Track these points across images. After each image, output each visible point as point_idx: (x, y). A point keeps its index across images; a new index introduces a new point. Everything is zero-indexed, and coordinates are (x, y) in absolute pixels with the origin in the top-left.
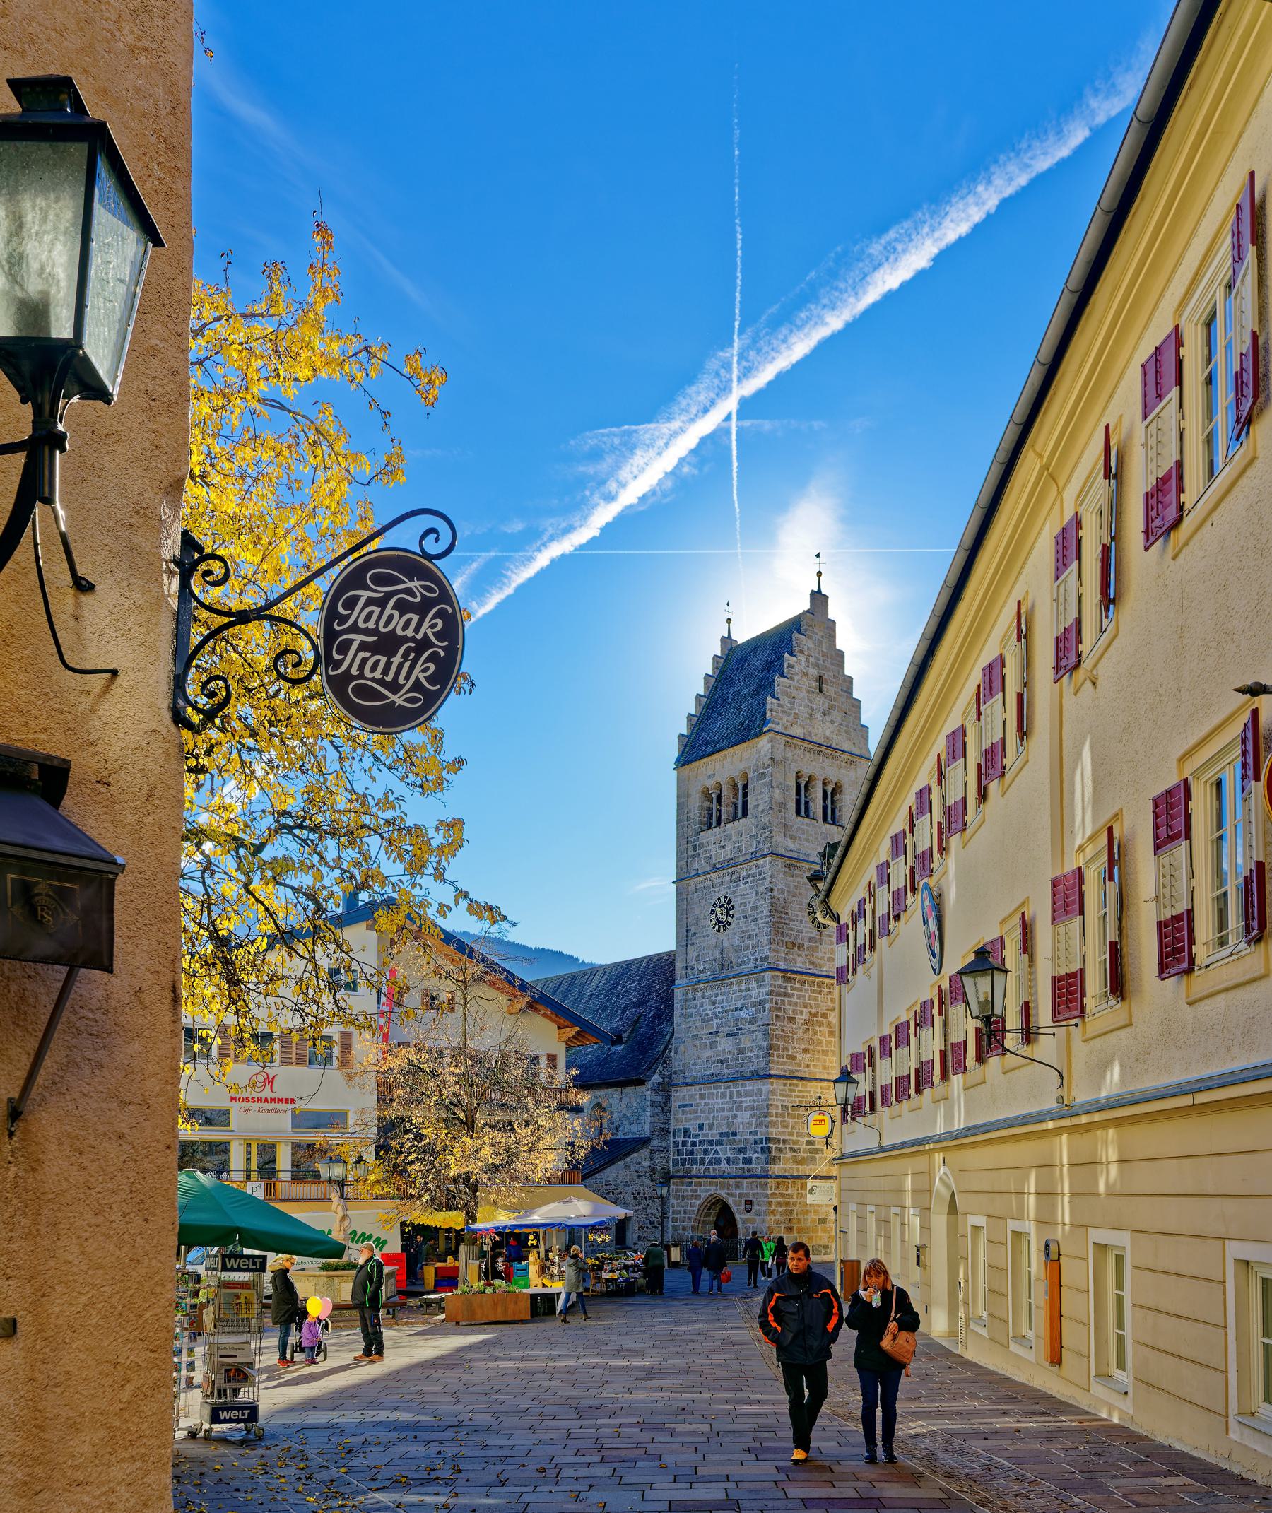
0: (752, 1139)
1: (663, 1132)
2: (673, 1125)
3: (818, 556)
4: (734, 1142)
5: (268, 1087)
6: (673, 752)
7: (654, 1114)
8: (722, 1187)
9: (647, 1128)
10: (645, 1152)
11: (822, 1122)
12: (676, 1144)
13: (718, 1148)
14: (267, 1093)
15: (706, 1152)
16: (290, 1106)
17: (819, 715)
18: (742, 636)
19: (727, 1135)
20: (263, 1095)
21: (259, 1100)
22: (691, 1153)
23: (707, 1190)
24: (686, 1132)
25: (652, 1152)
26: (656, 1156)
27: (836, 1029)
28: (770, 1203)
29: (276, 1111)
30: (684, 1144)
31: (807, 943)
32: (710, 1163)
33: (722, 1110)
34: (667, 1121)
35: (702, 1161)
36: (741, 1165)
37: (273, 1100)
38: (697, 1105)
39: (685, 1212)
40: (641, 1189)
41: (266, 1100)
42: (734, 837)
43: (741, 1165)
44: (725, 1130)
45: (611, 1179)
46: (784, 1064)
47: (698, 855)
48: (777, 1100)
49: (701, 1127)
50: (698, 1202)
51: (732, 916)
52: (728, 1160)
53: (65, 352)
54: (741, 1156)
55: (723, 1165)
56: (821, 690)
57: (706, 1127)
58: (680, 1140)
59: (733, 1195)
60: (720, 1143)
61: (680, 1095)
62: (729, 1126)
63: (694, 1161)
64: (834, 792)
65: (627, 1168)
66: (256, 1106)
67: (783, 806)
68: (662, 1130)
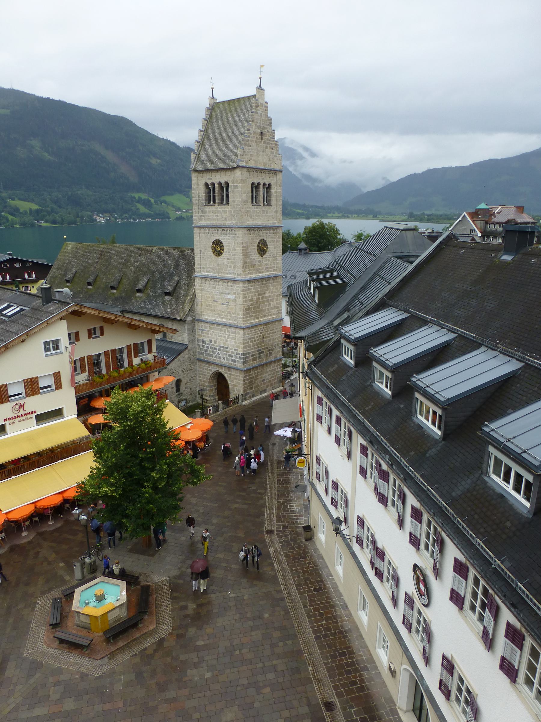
2: (197, 337)
3: (262, 66)
4: (226, 351)
5: (22, 409)
7: (189, 334)
8: (222, 369)
10: (186, 352)
12: (199, 345)
13: (219, 352)
14: (22, 412)
16: (34, 415)
17: (261, 153)
19: (223, 347)
20: (20, 414)
21: (18, 416)
22: (206, 351)
24: (203, 341)
26: (191, 351)
29: (28, 419)
31: (257, 263)
32: (216, 357)
33: (221, 336)
34: (194, 336)
35: (212, 356)
36: (230, 362)
38: (208, 331)
39: (204, 375)
40: (185, 368)
41: (22, 416)
43: (230, 362)
44: (222, 345)
46: (249, 320)
48: (240, 271)
49: (211, 341)
50: (211, 372)
52: (224, 358)
54: (230, 358)
55: (222, 360)
56: (262, 139)
57: (213, 342)
58: (201, 344)
59: (226, 373)
60: (219, 350)
61: (199, 326)
62: (224, 344)
63: (208, 355)
65: (179, 360)
66: (17, 420)
67: (247, 201)
68: (193, 340)
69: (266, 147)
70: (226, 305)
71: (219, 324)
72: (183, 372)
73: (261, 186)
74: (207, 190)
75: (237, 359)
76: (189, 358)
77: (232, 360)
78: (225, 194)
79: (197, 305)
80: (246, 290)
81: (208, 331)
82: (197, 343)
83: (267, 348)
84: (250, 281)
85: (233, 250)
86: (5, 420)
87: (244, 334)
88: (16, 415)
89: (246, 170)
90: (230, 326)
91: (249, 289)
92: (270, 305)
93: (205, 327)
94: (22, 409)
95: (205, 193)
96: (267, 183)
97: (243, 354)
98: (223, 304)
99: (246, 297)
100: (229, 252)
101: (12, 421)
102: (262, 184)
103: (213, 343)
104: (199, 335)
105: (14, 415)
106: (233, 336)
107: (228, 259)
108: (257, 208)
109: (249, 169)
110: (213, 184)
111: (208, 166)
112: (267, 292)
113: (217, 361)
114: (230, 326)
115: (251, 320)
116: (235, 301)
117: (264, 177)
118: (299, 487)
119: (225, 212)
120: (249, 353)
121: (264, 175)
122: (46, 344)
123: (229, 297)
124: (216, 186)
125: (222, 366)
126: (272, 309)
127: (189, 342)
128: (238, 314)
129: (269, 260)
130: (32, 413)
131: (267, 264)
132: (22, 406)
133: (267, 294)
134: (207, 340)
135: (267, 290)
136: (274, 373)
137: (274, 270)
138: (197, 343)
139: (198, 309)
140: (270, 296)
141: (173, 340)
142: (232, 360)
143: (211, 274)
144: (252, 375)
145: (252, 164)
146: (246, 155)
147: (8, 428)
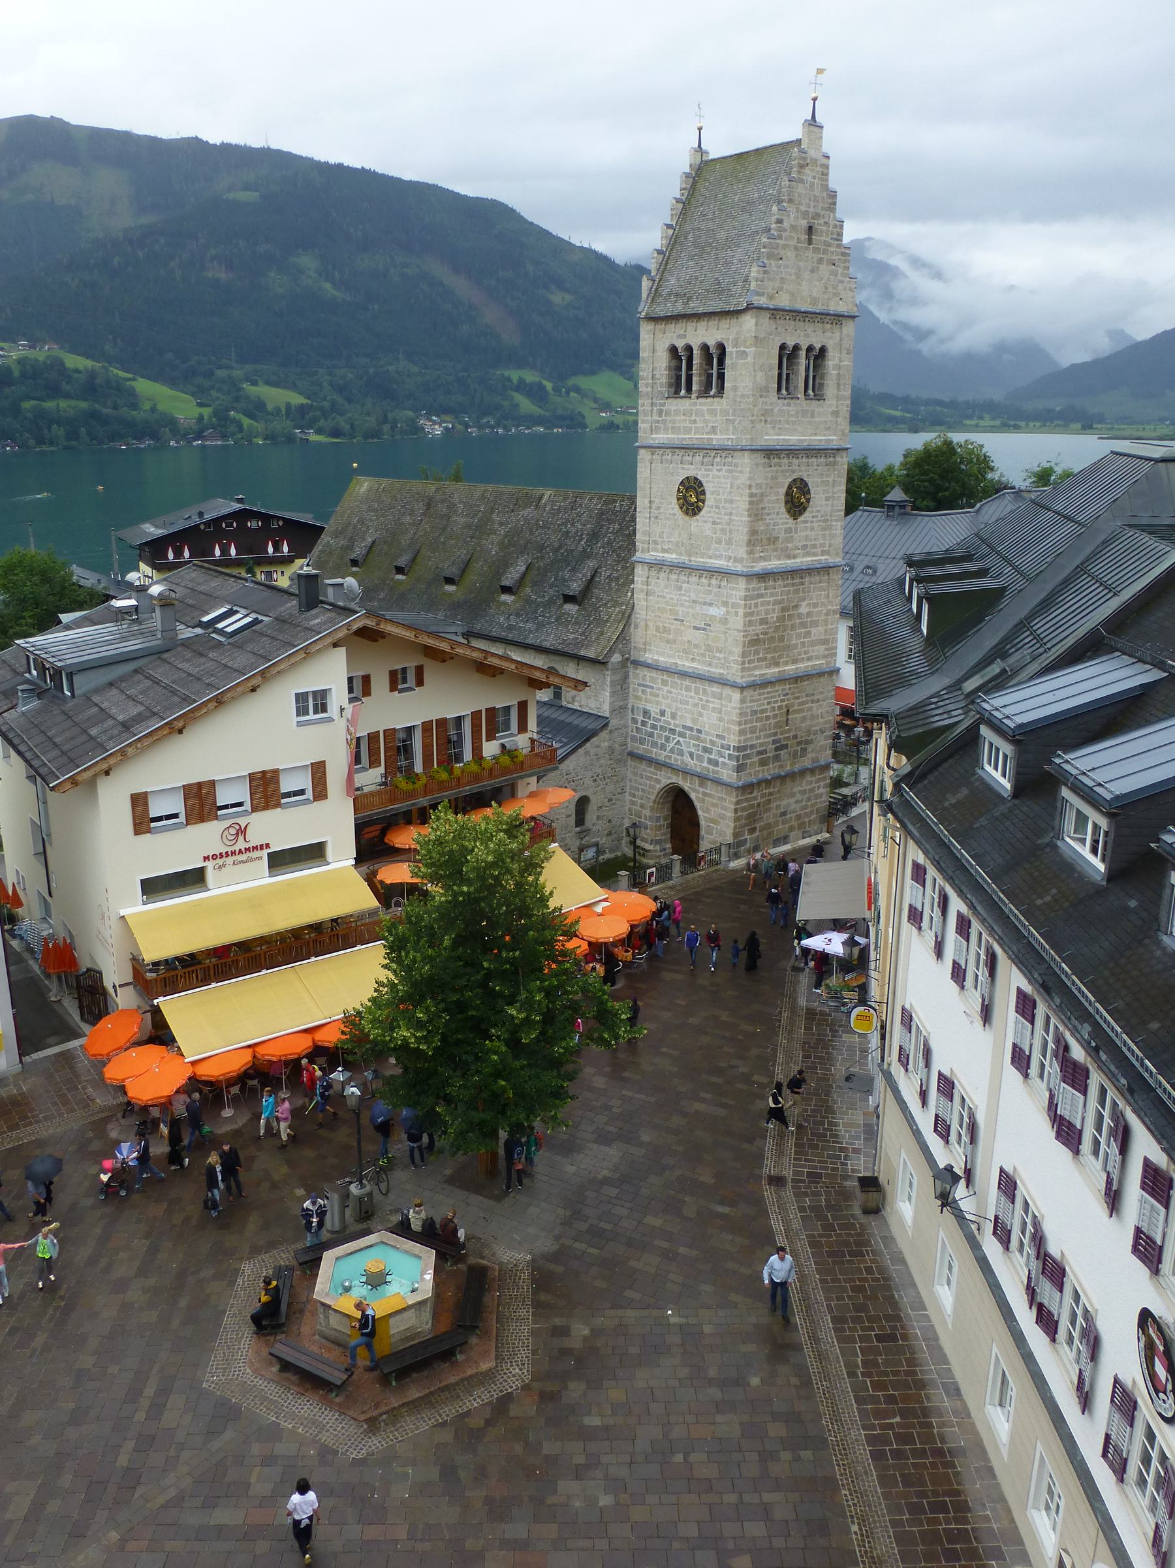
1: (620, 710)
4: (698, 739)
5: (241, 838)
7: (613, 694)
10: (604, 734)
12: (634, 721)
13: (681, 739)
15: (667, 739)
16: (265, 852)
17: (806, 275)
18: (717, 149)
19: (691, 729)
20: (236, 848)
21: (233, 853)
23: (666, 779)
24: (646, 713)
27: (991, 1246)
28: (769, 703)
29: (252, 860)
30: (644, 723)
31: (782, 535)
32: (672, 751)
33: (687, 703)
34: (625, 698)
35: (663, 747)
36: (705, 764)
37: (248, 850)
38: (659, 689)
43: (705, 764)
44: (689, 724)
45: (571, 768)
46: (755, 668)
47: (664, 422)
52: (691, 754)
53: (33, 982)
54: (707, 755)
55: (687, 758)
56: (810, 242)
58: (640, 718)
60: (682, 735)
62: (695, 721)
63: (654, 744)
64: (816, 358)
65: (587, 753)
66: (230, 860)
68: (621, 707)
69: (820, 261)
70: (704, 629)
71: (684, 674)
72: (595, 781)
73: (803, 353)
76: (611, 750)
77: (710, 761)
78: (714, 372)
79: (636, 627)
83: (795, 737)
84: (763, 576)
86: (206, 858)
87: (743, 701)
88: (229, 849)
89: (767, 314)
90: (712, 680)
92: (808, 634)
93: (652, 679)
94: (241, 838)
95: (669, 368)
96: (818, 346)
97: (738, 749)
99: (752, 614)
101: (220, 861)
103: (667, 718)
104: (636, 697)
105: (224, 850)
106: (715, 703)
109: (776, 313)
110: (689, 349)
111: (679, 308)
112: (804, 604)
113: (675, 760)
114: (712, 680)
116: (724, 621)
117: (809, 331)
119: (713, 412)
120: (752, 747)
121: (809, 327)
124: (696, 352)
125: (686, 773)
126: (813, 644)
127: (612, 711)
128: (731, 653)
130: (262, 847)
132: (242, 831)
133: (803, 609)
134: (654, 710)
135: (804, 600)
136: (809, 799)
137: (823, 553)
138: (630, 716)
139: (638, 636)
140: (809, 614)
142: (710, 761)
145: (784, 301)
147: (210, 875)
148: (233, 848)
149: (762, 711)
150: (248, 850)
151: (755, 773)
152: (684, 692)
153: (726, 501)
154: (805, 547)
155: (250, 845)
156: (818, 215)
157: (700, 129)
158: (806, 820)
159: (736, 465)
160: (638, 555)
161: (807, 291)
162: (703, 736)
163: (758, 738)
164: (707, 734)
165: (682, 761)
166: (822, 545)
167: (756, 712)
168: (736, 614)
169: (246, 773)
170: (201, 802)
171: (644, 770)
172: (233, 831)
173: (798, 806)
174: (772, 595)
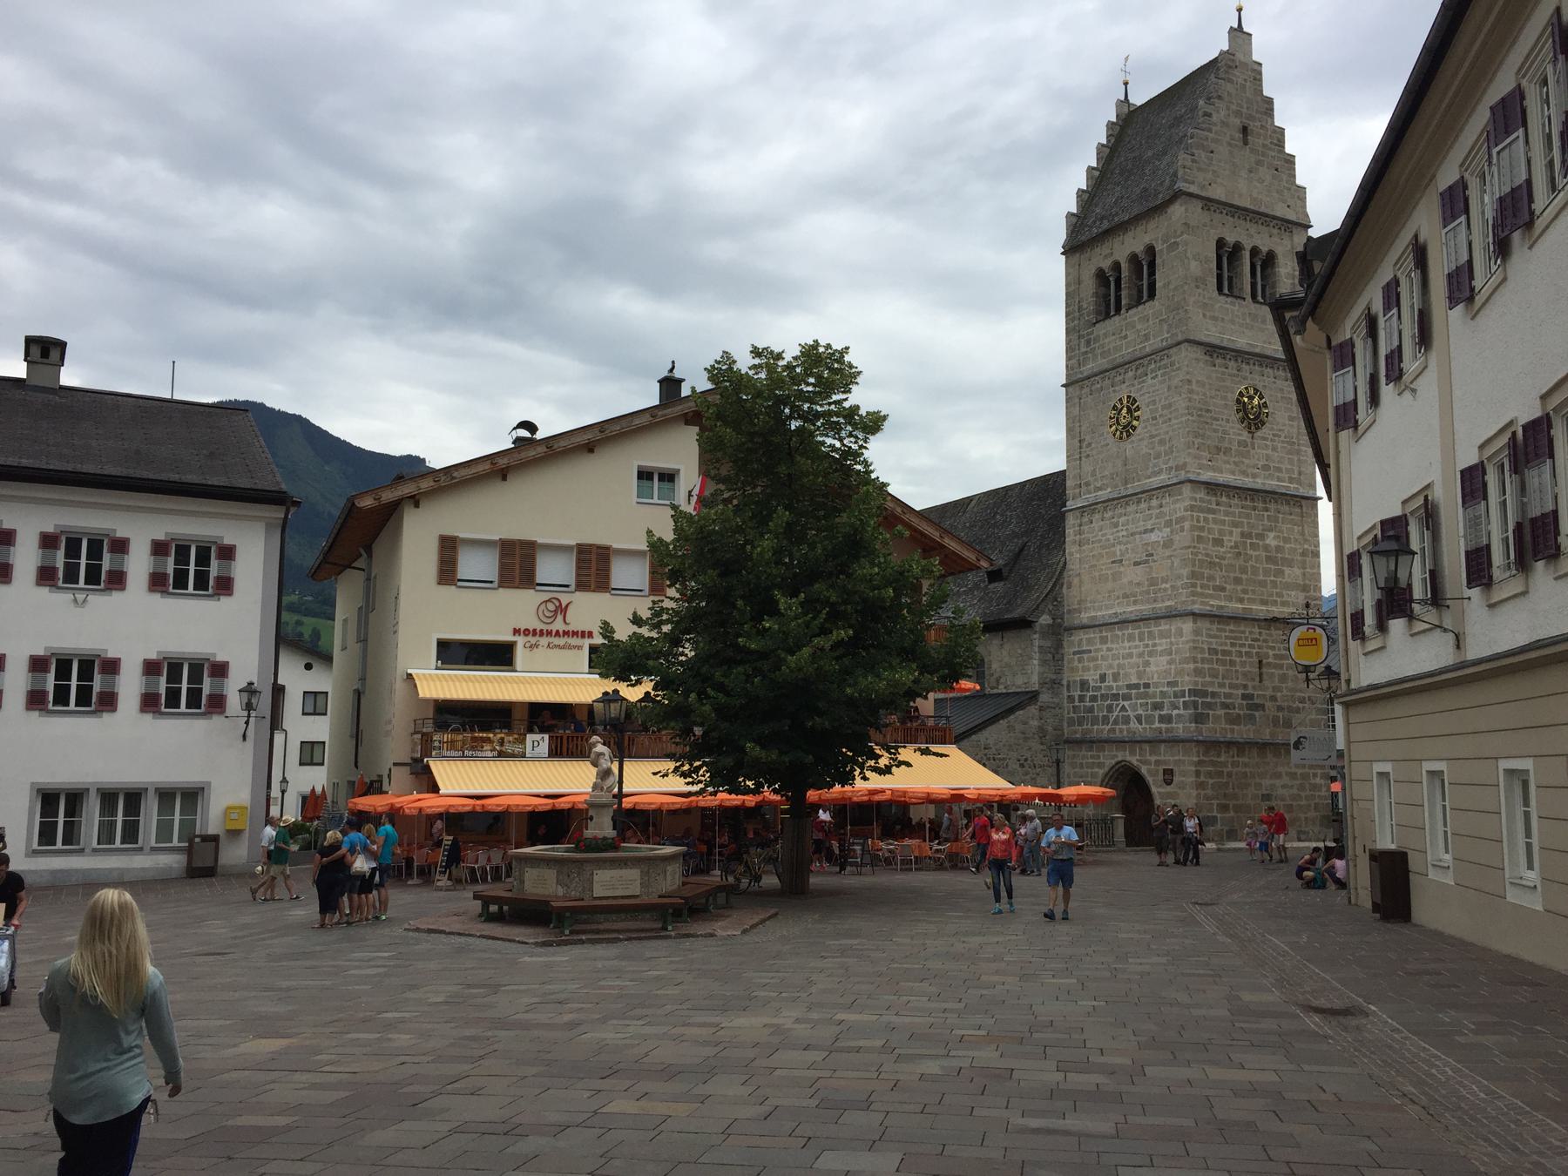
0: (1170, 690)
1: (1054, 684)
2: (1066, 677)
4: (1146, 695)
5: (560, 617)
6: (1061, 235)
7: (1043, 662)
9: (1035, 678)
10: (1033, 710)
11: (1313, 642)
12: (1071, 699)
13: (1126, 704)
14: (558, 625)
15: (1110, 709)
16: (587, 642)
17: (1244, 174)
19: (1137, 686)
21: (549, 633)
22: (1091, 710)
23: (1110, 758)
24: (1084, 685)
25: (1041, 709)
29: (570, 647)
30: (1082, 699)
31: (1235, 447)
32: (1116, 722)
33: (1130, 655)
34: (1059, 671)
35: (1106, 720)
36: (1157, 725)
37: (566, 633)
38: (1097, 650)
42: (1136, 328)
43: (1157, 725)
44: (1134, 681)
45: (991, 742)
46: (1211, 596)
49: (1103, 678)
50: (1101, 772)
51: (1137, 418)
52: (1139, 718)
55: (1134, 725)
56: (1246, 143)
57: (1110, 678)
58: (1077, 694)
60: (1127, 697)
62: (1140, 675)
63: (1095, 721)
65: (1011, 728)
66: (544, 641)
68: (1054, 682)
69: (1259, 163)
70: (1146, 562)
71: (1124, 623)
72: (1022, 766)
73: (1247, 255)
74: (1102, 290)
75: (1175, 712)
76: (1042, 731)
77: (1162, 719)
78: (1145, 282)
79: (1069, 587)
80: (1201, 510)
81: (1097, 650)
82: (1066, 694)
83: (1273, 698)
84: (1212, 487)
85: (1164, 408)
86: (516, 632)
87: (1196, 632)
88: (545, 627)
89: (1200, 204)
90: (1157, 618)
91: (1214, 512)
92: (1280, 573)
93: (1089, 641)
94: (560, 617)
95: (1096, 294)
96: (1265, 249)
97: (1193, 692)
98: (1136, 564)
99: (1202, 529)
100: (1154, 418)
101: (533, 640)
102: (1248, 247)
103: (1109, 682)
104: (1072, 670)
105: (539, 626)
106: (1163, 644)
107: (1152, 437)
108: (1232, 304)
109: (1209, 203)
110: (1117, 266)
111: (1106, 225)
112: (1272, 535)
113: (1122, 731)
114: (1157, 618)
115: (1219, 598)
116: (1168, 544)
117: (1252, 231)
118: (1306, 744)
119: (1146, 319)
120: (1214, 695)
121: (1253, 229)
122: (644, 475)
123: (1153, 537)
124: (1124, 266)
125: (1133, 742)
126: (1288, 586)
127: (1042, 684)
128: (1179, 577)
129: (1274, 449)
130: (583, 634)
131: (1268, 458)
132: (562, 610)
133: (1271, 540)
134: (1092, 677)
135: (1271, 530)
136: (1302, 788)
137: (1291, 480)
138: (1066, 694)
139: (1071, 596)
140: (1279, 549)
141: (1002, 689)
142: (1162, 719)
143: (1104, 494)
144: (1224, 764)
145: (1218, 193)
146: (1199, 169)
147: (520, 654)
148: (549, 627)
149: (1224, 653)
150: (566, 633)
151: (1216, 728)
152: (1126, 644)
153: (1164, 408)
154: (1266, 468)
155: (567, 628)
156: (1250, 117)
157: (1126, 84)
158: (1302, 816)
159: (1172, 364)
160: (1070, 504)
161: (1244, 192)
162: (1151, 690)
163: (1222, 685)
164: (1156, 685)
165: (1128, 730)
166: (1288, 471)
167: (1216, 652)
168: (1182, 530)
169: (573, 543)
170: (517, 563)
171: (1084, 757)
172: (551, 607)
173: (1285, 792)
174: (1227, 514)
